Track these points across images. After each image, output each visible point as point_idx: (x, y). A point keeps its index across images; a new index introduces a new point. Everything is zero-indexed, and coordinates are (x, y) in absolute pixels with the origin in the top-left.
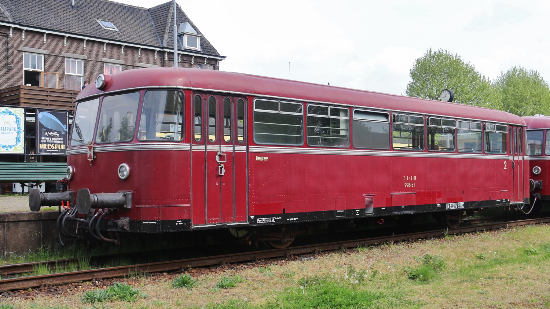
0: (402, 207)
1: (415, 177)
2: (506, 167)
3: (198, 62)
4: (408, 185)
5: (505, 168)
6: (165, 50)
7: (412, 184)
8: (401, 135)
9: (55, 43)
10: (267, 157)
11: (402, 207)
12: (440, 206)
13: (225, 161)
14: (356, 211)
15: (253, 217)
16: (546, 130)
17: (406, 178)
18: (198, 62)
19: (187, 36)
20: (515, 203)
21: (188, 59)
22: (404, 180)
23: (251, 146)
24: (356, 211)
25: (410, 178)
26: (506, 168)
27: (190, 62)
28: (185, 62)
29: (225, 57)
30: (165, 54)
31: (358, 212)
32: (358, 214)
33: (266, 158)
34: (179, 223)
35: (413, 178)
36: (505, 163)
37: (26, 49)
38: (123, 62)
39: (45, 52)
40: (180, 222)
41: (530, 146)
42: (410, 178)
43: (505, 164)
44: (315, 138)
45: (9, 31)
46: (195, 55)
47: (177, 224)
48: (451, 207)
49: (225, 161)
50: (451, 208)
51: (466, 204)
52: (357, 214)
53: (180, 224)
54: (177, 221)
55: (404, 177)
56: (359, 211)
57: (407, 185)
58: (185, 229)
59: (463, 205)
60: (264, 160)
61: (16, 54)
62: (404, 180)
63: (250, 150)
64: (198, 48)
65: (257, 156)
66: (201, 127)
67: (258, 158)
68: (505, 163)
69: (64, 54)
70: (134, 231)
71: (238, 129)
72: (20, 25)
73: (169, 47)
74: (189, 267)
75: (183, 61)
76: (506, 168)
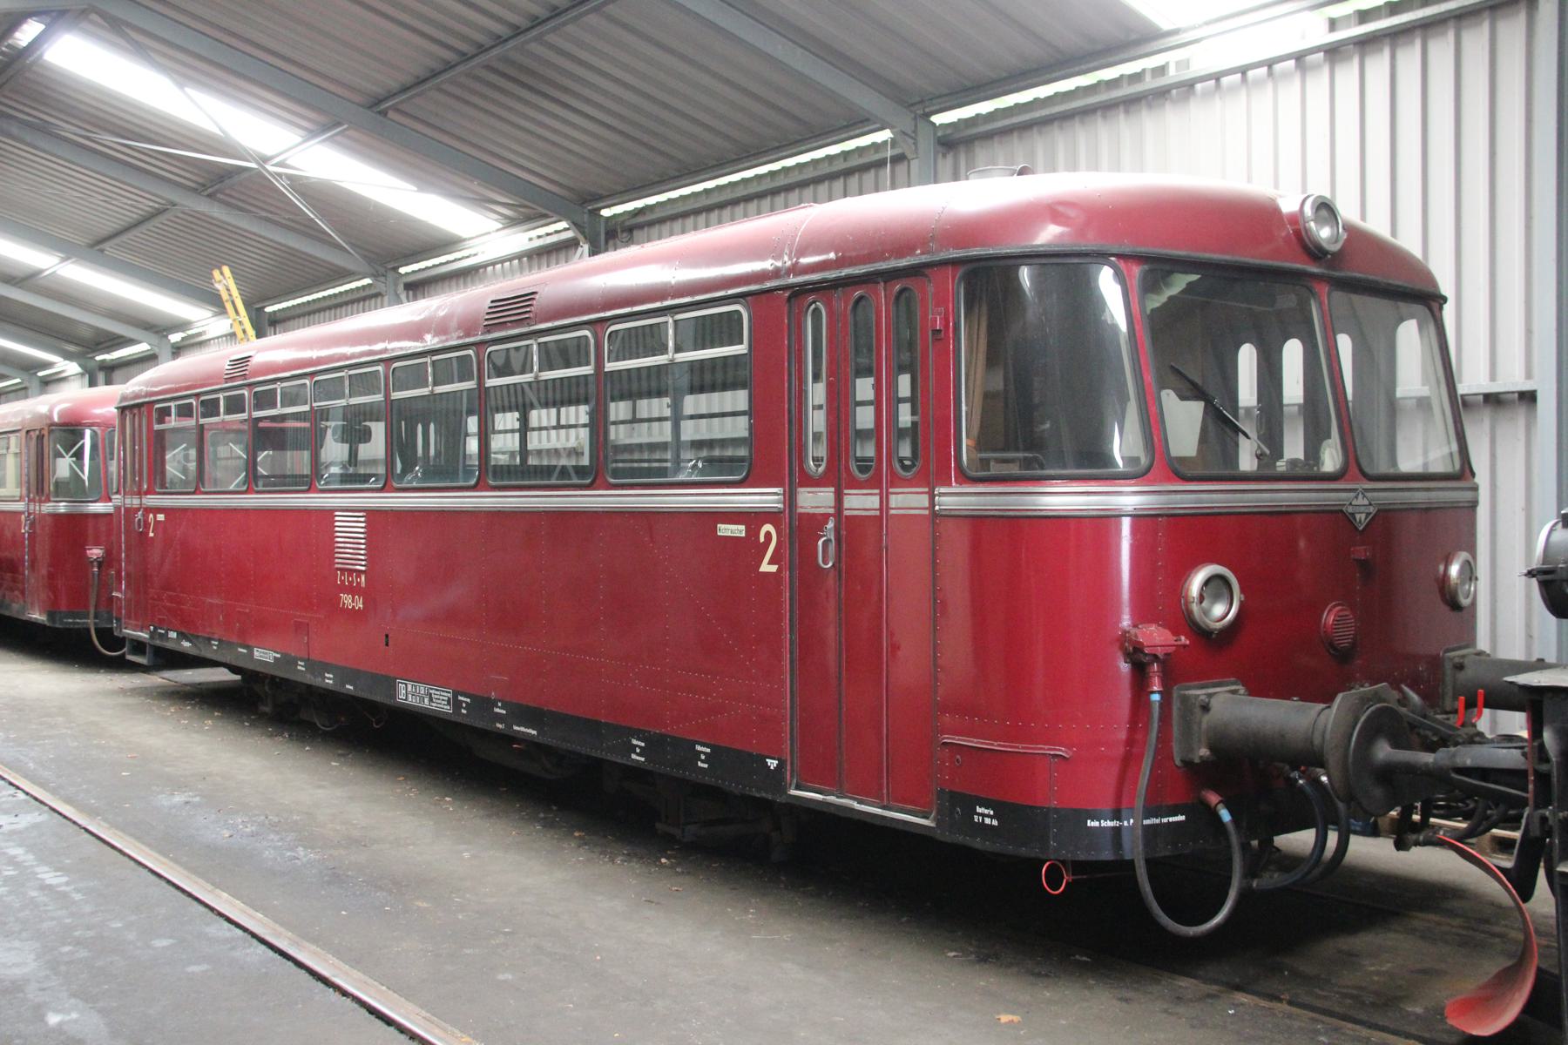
2: (770, 563)
5: (766, 567)
10: (742, 527)
13: (192, 403)
14: (699, 748)
15: (776, 762)
23: (943, 490)
24: (699, 748)
34: (984, 815)
36: (768, 535)
40: (988, 816)
41: (1534, 582)
43: (762, 539)
47: (976, 820)
49: (192, 403)
50: (411, 700)
53: (987, 821)
54: (979, 810)
56: (708, 750)
59: (449, 703)
68: (768, 535)
70: (694, 775)
74: (278, 841)
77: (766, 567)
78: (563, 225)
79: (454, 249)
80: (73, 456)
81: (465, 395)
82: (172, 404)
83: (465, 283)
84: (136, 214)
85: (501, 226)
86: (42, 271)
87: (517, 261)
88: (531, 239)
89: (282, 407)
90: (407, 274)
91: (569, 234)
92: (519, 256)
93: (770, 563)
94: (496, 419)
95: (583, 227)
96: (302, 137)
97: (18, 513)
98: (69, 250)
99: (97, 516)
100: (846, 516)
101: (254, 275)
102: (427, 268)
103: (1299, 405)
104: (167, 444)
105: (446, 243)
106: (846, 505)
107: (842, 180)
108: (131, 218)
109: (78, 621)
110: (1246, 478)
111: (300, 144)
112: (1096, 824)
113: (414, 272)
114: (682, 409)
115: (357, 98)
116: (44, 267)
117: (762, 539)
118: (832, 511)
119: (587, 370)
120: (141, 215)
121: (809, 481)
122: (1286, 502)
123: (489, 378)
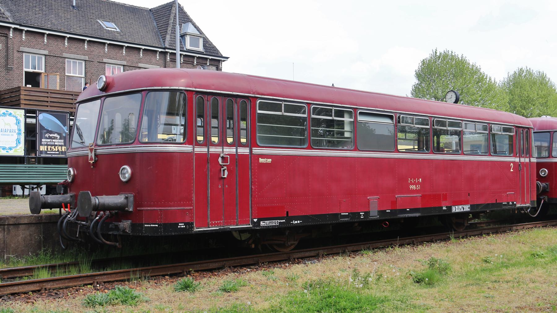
0: (407, 210)
1: (420, 180)
2: (512, 170)
3: (201, 63)
4: (413, 188)
5: (512, 170)
6: (167, 50)
7: (417, 187)
8: (406, 137)
9: (56, 44)
10: (271, 159)
11: (407, 210)
12: (446, 209)
13: (228, 163)
14: (361, 213)
15: (256, 220)
16: (553, 132)
17: (411, 180)
18: (201, 63)
19: (190, 37)
20: (522, 205)
21: (191, 60)
22: (409, 182)
23: (254, 148)
24: (361, 213)
25: (415, 180)
26: (512, 171)
27: (192, 63)
28: (188, 62)
29: (228, 58)
30: (167, 55)
31: (362, 215)
32: (363, 217)
33: (269, 161)
34: (181, 225)
35: (418, 180)
36: (512, 165)
37: (26, 49)
38: (125, 63)
39: (46, 52)
40: (182, 225)
41: (537, 147)
42: (415, 180)
43: (511, 166)
44: (319, 139)
45: (10, 31)
46: (198, 55)
47: (179, 227)
48: (457, 210)
49: (228, 163)
50: (457, 211)
51: (472, 207)
52: (361, 217)
53: (182, 227)
54: (180, 224)
55: (409, 179)
56: (364, 213)
57: (413, 187)
58: (188, 232)
59: (469, 208)
60: (268, 162)
61: (16, 54)
62: (409, 182)
63: (253, 152)
64: (201, 49)
65: (260, 158)
66: (204, 129)
67: (261, 160)
68: (512, 165)
69: (65, 55)
70: (135, 234)
71: (241, 130)
72: (21, 25)
73: (171, 47)
75: (185, 62)
76: (512, 171)
82: (283, 104)
106: (210, 151)
119: (305, 116)
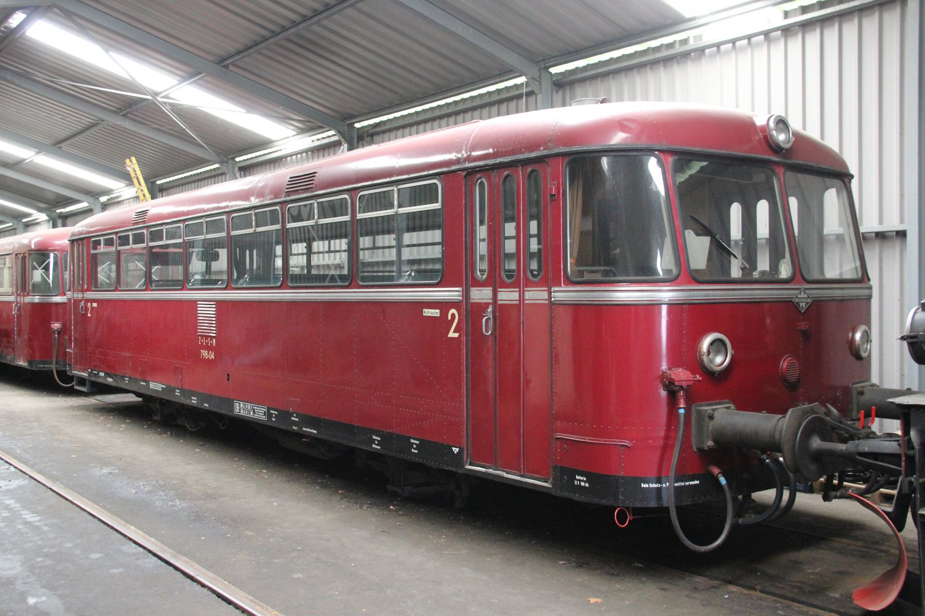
2: (454, 332)
5: (452, 334)
10: (438, 311)
13: (113, 238)
14: (412, 441)
15: (458, 449)
24: (412, 441)
34: (580, 481)
36: (453, 315)
40: (583, 481)
41: (905, 343)
43: (449, 318)
47: (576, 484)
49: (113, 238)
50: (243, 413)
53: (583, 484)
54: (578, 477)
56: (418, 442)
59: (265, 415)
63: (553, 299)
66: (505, 268)
68: (453, 315)
77: (452, 334)
78: (332, 132)
79: (268, 147)
80: (43, 269)
81: (274, 233)
83: (274, 167)
84: (81, 126)
85: (295, 133)
86: (25, 160)
87: (305, 154)
88: (313, 141)
89: (166, 240)
90: (240, 161)
91: (336, 138)
92: (306, 151)
93: (454, 332)
94: (292, 247)
95: (344, 134)
96: (178, 81)
97: (11, 303)
98: (41, 147)
99: (57, 304)
100: (499, 304)
101: (150, 162)
102: (252, 158)
103: (766, 239)
104: (99, 262)
105: (263, 144)
107: (497, 106)
108: (77, 128)
109: (46, 366)
110: (735, 282)
111: (177, 85)
112: (646, 486)
113: (244, 160)
114: (402, 241)
115: (211, 58)
116: (26, 158)
117: (449, 318)
118: (491, 301)
120: (83, 127)
121: (477, 284)
122: (759, 296)
123: (288, 223)
